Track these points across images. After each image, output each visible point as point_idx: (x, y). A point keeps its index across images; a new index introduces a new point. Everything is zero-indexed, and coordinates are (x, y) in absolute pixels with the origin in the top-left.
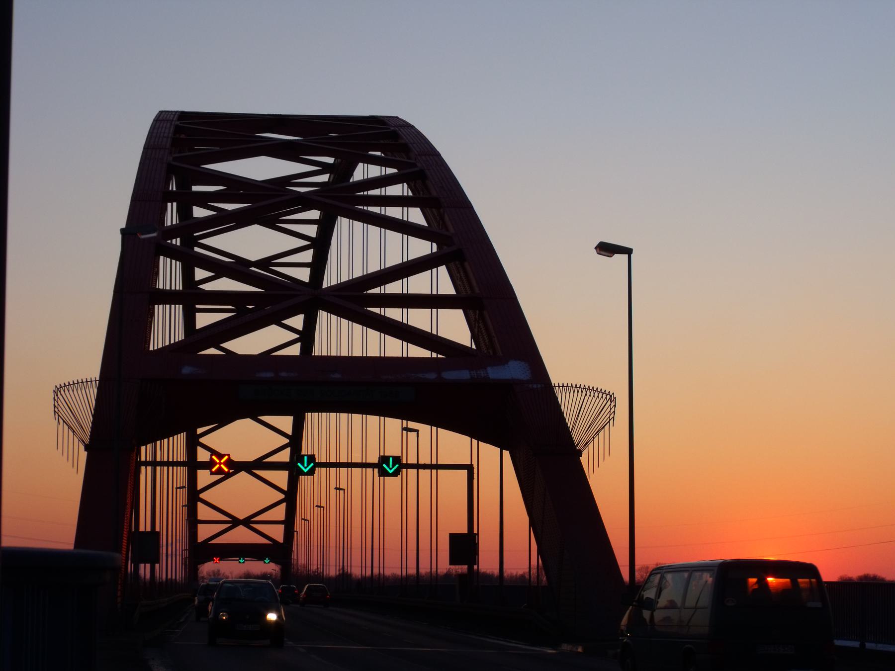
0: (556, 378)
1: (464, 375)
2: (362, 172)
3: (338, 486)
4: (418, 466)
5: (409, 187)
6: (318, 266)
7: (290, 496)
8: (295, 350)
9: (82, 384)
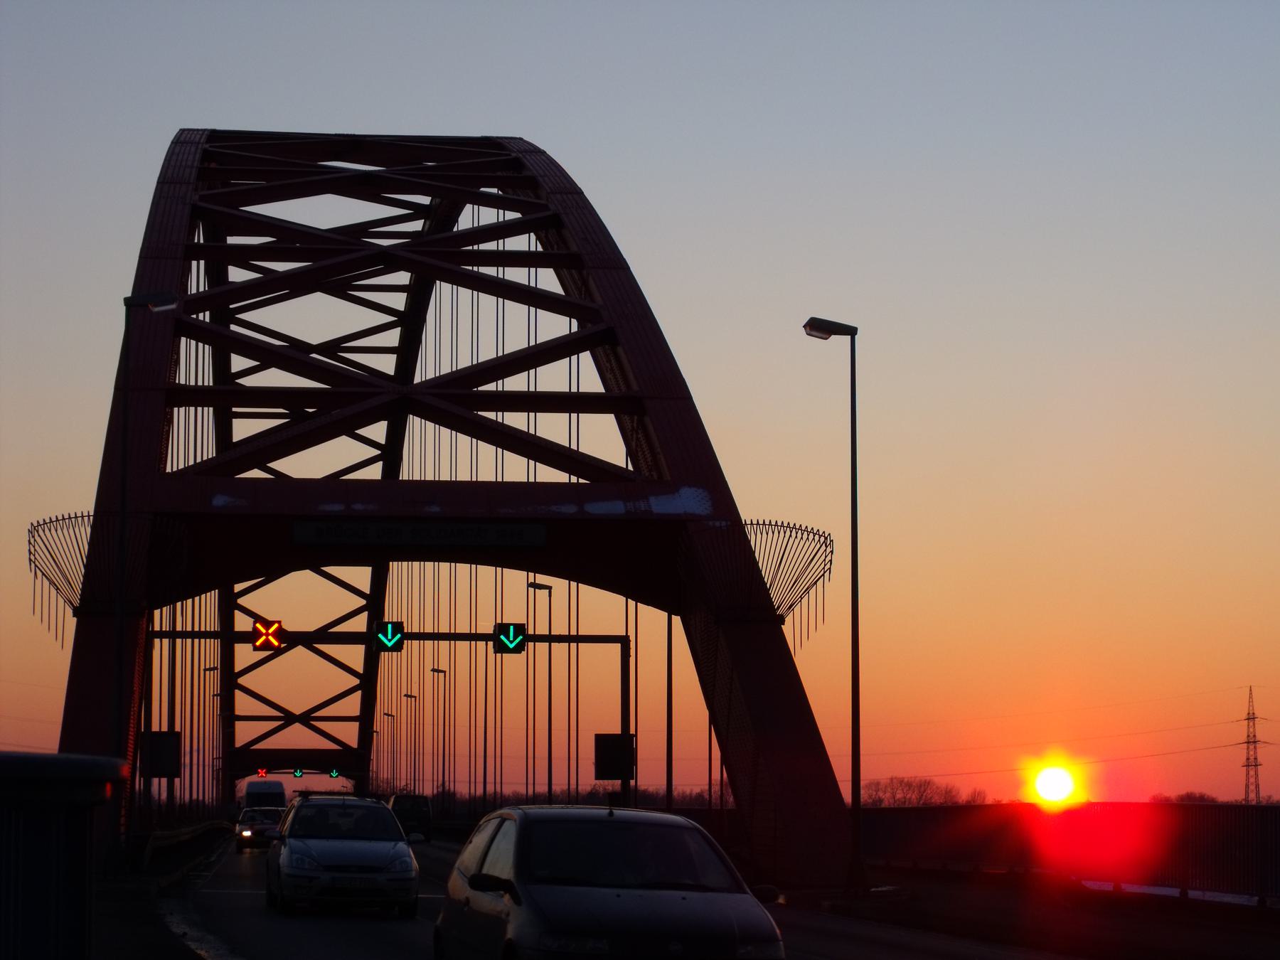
0: (749, 506)
1: (616, 507)
2: (470, 218)
3: (436, 667)
4: (550, 639)
5: (538, 238)
6: (408, 352)
7: (368, 682)
8: (374, 472)
9: (69, 520)
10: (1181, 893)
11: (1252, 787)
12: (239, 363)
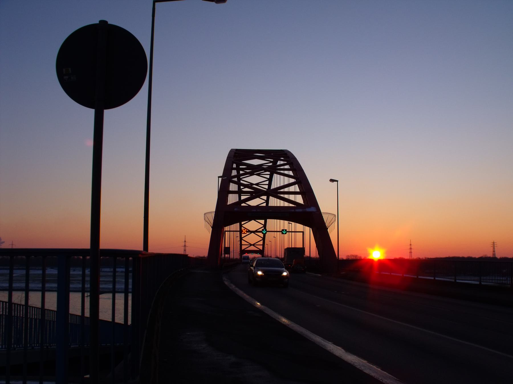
0: (322, 211)
1: (301, 210)
2: (279, 163)
4: (292, 232)
5: (290, 167)
6: (270, 185)
7: (264, 239)
8: (265, 205)
10: (480, 283)
11: (411, 256)
12: (242, 187)
